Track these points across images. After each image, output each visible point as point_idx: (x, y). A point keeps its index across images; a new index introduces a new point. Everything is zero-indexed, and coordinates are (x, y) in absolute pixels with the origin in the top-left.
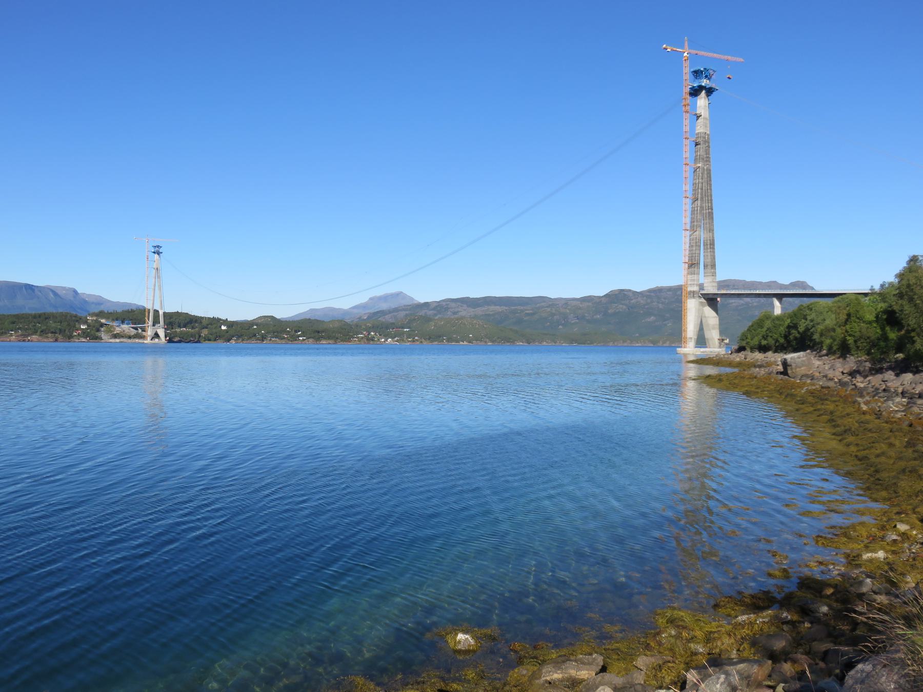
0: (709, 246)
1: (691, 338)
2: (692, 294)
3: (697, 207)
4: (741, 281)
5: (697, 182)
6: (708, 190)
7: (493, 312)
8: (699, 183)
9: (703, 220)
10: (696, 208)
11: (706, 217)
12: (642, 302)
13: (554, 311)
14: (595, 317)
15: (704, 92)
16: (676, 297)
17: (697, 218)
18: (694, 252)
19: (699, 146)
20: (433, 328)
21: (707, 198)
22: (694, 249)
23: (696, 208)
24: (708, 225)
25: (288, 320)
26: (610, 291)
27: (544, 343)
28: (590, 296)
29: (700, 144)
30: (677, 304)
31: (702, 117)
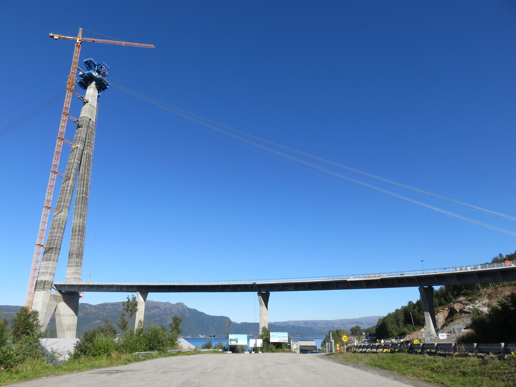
0: (77, 233)
2: (42, 285)
3: (68, 186)
5: (73, 161)
6: (85, 174)
8: (74, 163)
9: (76, 204)
10: (66, 188)
11: (79, 201)
12: (94, 311)
15: (94, 83)
16: (114, 309)
17: (65, 198)
18: (54, 235)
19: (81, 129)
21: (82, 182)
22: (56, 231)
23: (66, 188)
24: (79, 211)
25: (379, 325)
29: (82, 126)
31: (89, 103)
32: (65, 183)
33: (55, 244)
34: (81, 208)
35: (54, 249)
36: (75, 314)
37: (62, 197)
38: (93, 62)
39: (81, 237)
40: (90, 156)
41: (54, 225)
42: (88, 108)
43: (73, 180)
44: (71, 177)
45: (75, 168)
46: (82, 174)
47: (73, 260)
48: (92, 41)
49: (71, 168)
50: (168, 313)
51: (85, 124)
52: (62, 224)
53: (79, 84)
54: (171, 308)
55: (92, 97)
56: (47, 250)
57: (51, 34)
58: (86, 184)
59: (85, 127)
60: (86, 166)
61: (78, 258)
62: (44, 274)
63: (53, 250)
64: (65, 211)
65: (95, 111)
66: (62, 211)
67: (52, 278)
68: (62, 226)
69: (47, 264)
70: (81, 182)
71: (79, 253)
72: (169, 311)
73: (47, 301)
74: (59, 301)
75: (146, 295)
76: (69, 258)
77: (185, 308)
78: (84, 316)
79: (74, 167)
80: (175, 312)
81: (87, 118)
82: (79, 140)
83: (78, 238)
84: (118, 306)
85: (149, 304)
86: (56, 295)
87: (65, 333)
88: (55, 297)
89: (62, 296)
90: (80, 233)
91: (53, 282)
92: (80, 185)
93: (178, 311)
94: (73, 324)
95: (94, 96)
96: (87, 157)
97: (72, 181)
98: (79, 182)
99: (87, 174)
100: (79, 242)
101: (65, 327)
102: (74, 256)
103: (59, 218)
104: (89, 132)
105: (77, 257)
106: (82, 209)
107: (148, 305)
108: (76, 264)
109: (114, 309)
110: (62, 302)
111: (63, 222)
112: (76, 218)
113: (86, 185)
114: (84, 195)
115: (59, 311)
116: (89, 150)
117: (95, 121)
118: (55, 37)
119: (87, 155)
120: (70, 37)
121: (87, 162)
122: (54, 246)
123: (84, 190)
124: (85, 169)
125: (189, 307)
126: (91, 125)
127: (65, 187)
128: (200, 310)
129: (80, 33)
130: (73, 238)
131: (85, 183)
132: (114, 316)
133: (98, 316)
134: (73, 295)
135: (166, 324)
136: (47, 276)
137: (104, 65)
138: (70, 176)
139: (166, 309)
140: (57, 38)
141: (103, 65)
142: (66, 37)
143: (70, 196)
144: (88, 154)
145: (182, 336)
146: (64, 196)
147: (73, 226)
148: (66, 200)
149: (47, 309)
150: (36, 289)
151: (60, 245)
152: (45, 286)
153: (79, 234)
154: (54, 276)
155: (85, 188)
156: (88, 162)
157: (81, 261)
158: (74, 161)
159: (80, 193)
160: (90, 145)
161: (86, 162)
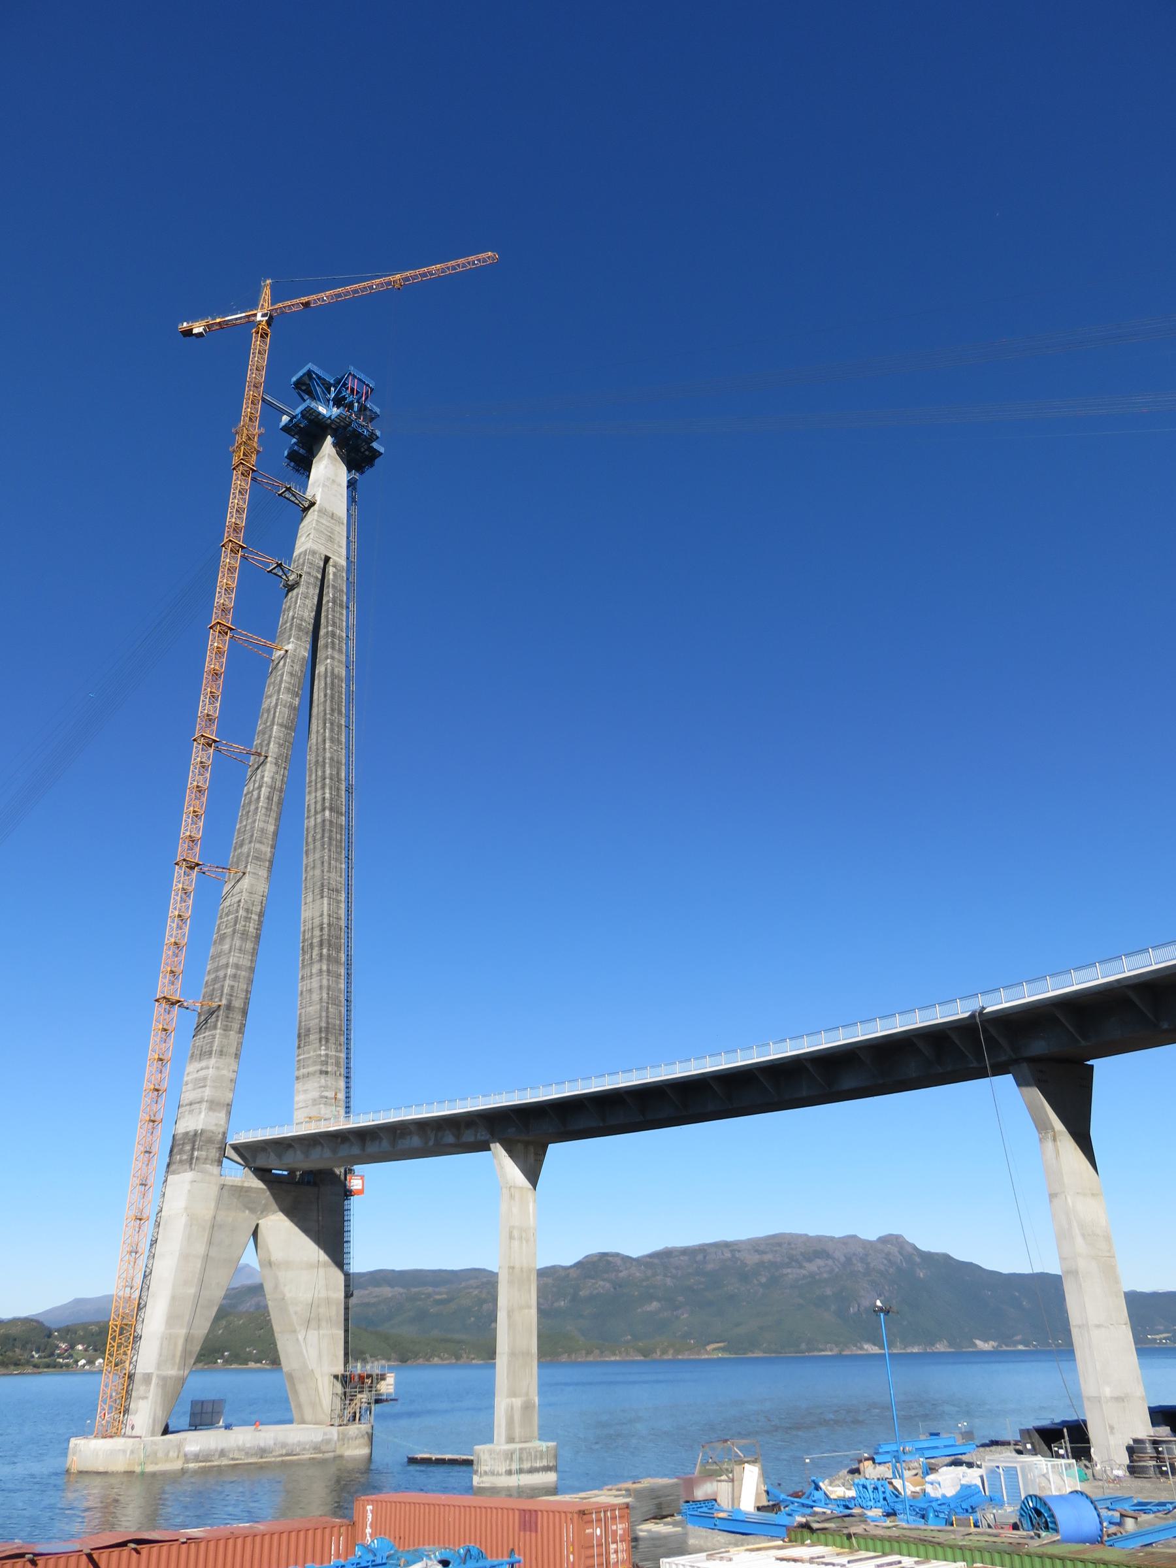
0: (316, 951)
1: (147, 1378)
2: (188, 1148)
4: (801, 1235)
6: (324, 741)
7: (375, 1300)
10: (255, 793)
12: (638, 1274)
13: (484, 1296)
14: (556, 1305)
16: (695, 1265)
17: (253, 828)
18: (223, 961)
20: (220, 1332)
21: (320, 773)
24: (318, 872)
26: (583, 1256)
27: (436, 1359)
28: (553, 1267)
30: (697, 1278)
31: (316, 507)
32: (253, 778)
33: (225, 991)
34: (323, 863)
35: (221, 1012)
36: (330, 1261)
37: (246, 826)
38: (319, 377)
39: (328, 965)
40: (336, 681)
41: (224, 927)
42: (314, 522)
43: (275, 764)
44: (270, 754)
45: (280, 721)
46: (317, 743)
47: (312, 1054)
48: (302, 304)
49: (268, 724)
50: (859, 1271)
51: (309, 574)
52: (247, 919)
53: (292, 464)
54: (867, 1255)
55: (324, 485)
56: (203, 1018)
57: (185, 324)
58: (331, 774)
59: (309, 583)
60: (325, 714)
61: (323, 1043)
62: (193, 1107)
63: (218, 1016)
64: (255, 874)
65: (342, 531)
66: (244, 873)
67: (223, 1122)
68: (245, 926)
69: (202, 1069)
70: (316, 771)
71: (328, 1023)
72: (859, 1265)
73: (206, 1211)
74: (262, 1212)
75: (536, 1154)
76: (299, 1047)
77: (910, 1250)
78: (612, 1290)
79: (276, 720)
80: (882, 1268)
81: (314, 553)
82: (291, 629)
83: (321, 971)
84: (705, 1257)
85: (795, 1244)
86: (242, 1187)
87: (301, 1337)
88: (240, 1196)
89: (270, 1188)
90: (325, 951)
91: (224, 1134)
92: (313, 784)
93: (890, 1261)
94: (328, 1301)
95: (334, 481)
96: (326, 684)
97: (274, 768)
98: (310, 776)
99: (332, 740)
100: (325, 982)
101: (296, 1313)
102: (312, 1037)
103: (235, 899)
104: (328, 602)
105: (320, 1041)
106: (326, 865)
107: (792, 1249)
108: (318, 1067)
109: (695, 1265)
110: (274, 1212)
111: (247, 910)
112: (311, 899)
113: (331, 779)
114: (327, 813)
115: (268, 1251)
116: (333, 658)
117: (344, 563)
118: (195, 331)
119: (326, 678)
120: (237, 314)
121: (328, 701)
122: (221, 1000)
123: (327, 796)
124: (325, 724)
125: (923, 1249)
126: (331, 577)
127: (253, 791)
128: (961, 1254)
129: (266, 293)
130: (307, 971)
131: (328, 772)
132: (695, 1287)
133: (651, 1291)
134: (315, 1184)
135: (859, 1306)
136: (200, 1113)
137: (354, 377)
138: (267, 751)
139: (849, 1260)
140: (201, 330)
141: (350, 378)
142: (227, 319)
143: (272, 821)
144: (329, 674)
145: (919, 1345)
146: (250, 821)
147: (304, 931)
148: (255, 835)
149: (210, 1243)
150: (173, 1168)
151: (243, 995)
152: (196, 1153)
153: (321, 955)
154: (229, 1113)
155: (327, 791)
156: (331, 701)
157: (337, 1054)
158: (277, 700)
159: (315, 811)
160: (333, 643)
161: (325, 701)
